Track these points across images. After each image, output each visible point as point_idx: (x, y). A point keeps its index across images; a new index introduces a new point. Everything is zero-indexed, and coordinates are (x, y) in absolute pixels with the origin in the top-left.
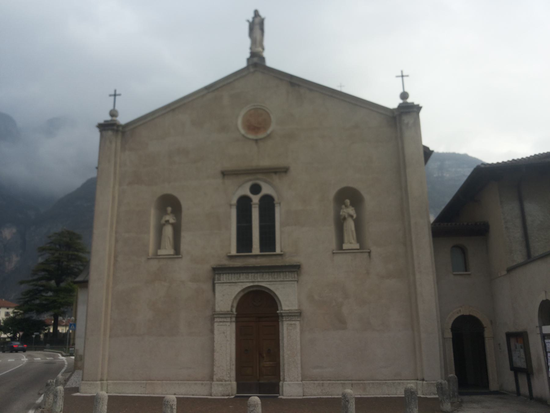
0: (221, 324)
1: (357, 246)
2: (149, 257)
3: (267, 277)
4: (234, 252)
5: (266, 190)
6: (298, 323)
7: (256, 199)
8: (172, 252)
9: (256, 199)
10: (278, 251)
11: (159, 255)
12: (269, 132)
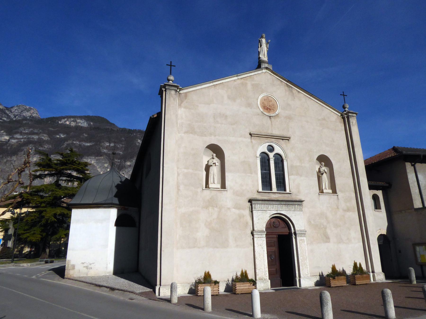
0: (259, 239)
1: (330, 191)
2: (259, 191)
3: (284, 207)
4: (260, 190)
5: (278, 150)
6: (305, 238)
8: (219, 186)
9: (271, 155)
10: (288, 191)
11: (210, 188)
12: (277, 113)
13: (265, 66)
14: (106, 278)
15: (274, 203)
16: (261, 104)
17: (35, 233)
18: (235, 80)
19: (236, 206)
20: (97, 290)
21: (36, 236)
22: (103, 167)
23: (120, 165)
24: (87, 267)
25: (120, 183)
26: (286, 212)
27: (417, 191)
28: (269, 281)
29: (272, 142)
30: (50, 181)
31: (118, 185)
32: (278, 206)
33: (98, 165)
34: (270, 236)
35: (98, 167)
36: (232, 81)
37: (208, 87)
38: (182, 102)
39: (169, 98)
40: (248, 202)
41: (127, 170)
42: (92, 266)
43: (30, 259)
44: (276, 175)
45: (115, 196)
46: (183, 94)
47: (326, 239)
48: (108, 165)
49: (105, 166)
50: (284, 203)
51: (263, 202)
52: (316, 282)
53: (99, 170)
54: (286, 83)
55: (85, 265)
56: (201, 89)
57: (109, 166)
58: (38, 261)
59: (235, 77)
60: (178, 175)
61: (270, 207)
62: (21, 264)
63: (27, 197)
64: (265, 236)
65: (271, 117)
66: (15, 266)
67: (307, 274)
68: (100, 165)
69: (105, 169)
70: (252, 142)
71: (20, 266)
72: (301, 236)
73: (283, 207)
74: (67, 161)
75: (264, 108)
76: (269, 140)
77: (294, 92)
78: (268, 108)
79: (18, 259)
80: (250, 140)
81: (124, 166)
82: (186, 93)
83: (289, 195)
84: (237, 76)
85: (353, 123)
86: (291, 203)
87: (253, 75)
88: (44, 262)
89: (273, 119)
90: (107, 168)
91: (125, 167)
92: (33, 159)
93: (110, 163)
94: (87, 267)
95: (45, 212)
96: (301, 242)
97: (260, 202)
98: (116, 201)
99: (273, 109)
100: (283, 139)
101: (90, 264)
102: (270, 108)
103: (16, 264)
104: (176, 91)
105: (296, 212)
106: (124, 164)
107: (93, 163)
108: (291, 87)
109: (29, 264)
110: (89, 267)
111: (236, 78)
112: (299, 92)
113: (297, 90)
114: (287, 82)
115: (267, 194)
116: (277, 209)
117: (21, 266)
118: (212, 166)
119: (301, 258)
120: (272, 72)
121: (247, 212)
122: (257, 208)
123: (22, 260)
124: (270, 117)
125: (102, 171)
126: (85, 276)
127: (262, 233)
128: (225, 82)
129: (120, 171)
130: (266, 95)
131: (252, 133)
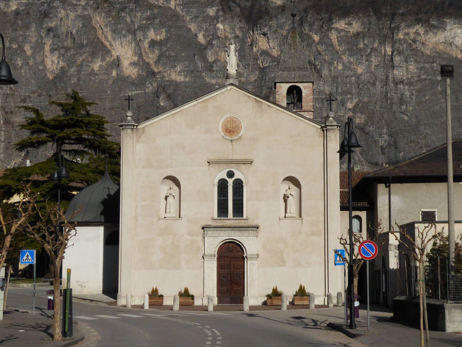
0: (209, 262)
3: (237, 233)
4: (216, 216)
5: (238, 175)
7: (230, 182)
9: (230, 182)
10: (245, 216)
12: (240, 135)
13: (229, 82)
14: (99, 295)
15: (226, 229)
16: (222, 127)
17: (33, 240)
18: (194, 105)
19: (190, 233)
20: (83, 302)
21: (35, 245)
22: (204, 17)
23: (252, 6)
24: (81, 285)
25: (107, 197)
26: (238, 237)
27: (387, 215)
28: (217, 298)
29: (232, 168)
30: (62, 68)
31: (105, 200)
32: (231, 232)
33: (188, 13)
34: (221, 259)
35: (188, 18)
36: (190, 106)
37: (166, 117)
38: (140, 137)
39: (126, 137)
40: (202, 229)
41: (274, 23)
42: (85, 284)
43: (31, 279)
44: (234, 200)
45: (101, 214)
46: (141, 129)
47: (283, 262)
48: (218, 10)
49: (208, 16)
50: (237, 229)
51: (216, 229)
52: (264, 302)
53: (193, 27)
54: (254, 97)
55: (80, 283)
56: (159, 120)
57: (221, 13)
58: (41, 281)
59: (194, 101)
60: (136, 207)
61: (222, 233)
62: (20, 284)
63: (16, 186)
64: (216, 259)
65: (233, 141)
66: (14, 286)
67: (254, 294)
68: (194, 10)
69: (210, 25)
70: (209, 170)
71: (19, 287)
72: (252, 260)
73: (236, 233)
74: (69, 121)
75: (226, 131)
76: (229, 166)
77: (264, 107)
78: (231, 130)
79: (15, 278)
80: (207, 168)
81: (266, 9)
82: (144, 128)
83: (246, 221)
84: (196, 100)
85: (330, 137)
86: (244, 229)
87: (216, 95)
88: (48, 283)
89: (234, 143)
90: (215, 21)
91: (267, 12)
92: (10, 6)
93: (221, 5)
94: (81, 285)
95: (44, 210)
96: (252, 265)
97: (212, 229)
98: (102, 219)
99: (236, 131)
100: (244, 164)
101: (84, 283)
102: (233, 130)
103: (14, 285)
104: (132, 129)
105: (249, 237)
106: (264, 5)
107: (173, 8)
108: (261, 102)
109: (30, 285)
110: (83, 285)
111: (196, 102)
112: (269, 106)
113: (267, 105)
114: (256, 96)
115: (222, 221)
116: (229, 235)
117: (21, 287)
118: (169, 196)
119: (250, 280)
120: (238, 88)
121: (200, 238)
122: (209, 235)
123: (19, 280)
124: (232, 140)
125: (200, 31)
126: (80, 293)
127: (212, 257)
128: (185, 109)
129: (253, 27)
130: (230, 116)
131: (209, 161)
